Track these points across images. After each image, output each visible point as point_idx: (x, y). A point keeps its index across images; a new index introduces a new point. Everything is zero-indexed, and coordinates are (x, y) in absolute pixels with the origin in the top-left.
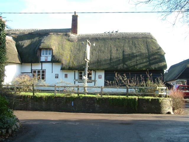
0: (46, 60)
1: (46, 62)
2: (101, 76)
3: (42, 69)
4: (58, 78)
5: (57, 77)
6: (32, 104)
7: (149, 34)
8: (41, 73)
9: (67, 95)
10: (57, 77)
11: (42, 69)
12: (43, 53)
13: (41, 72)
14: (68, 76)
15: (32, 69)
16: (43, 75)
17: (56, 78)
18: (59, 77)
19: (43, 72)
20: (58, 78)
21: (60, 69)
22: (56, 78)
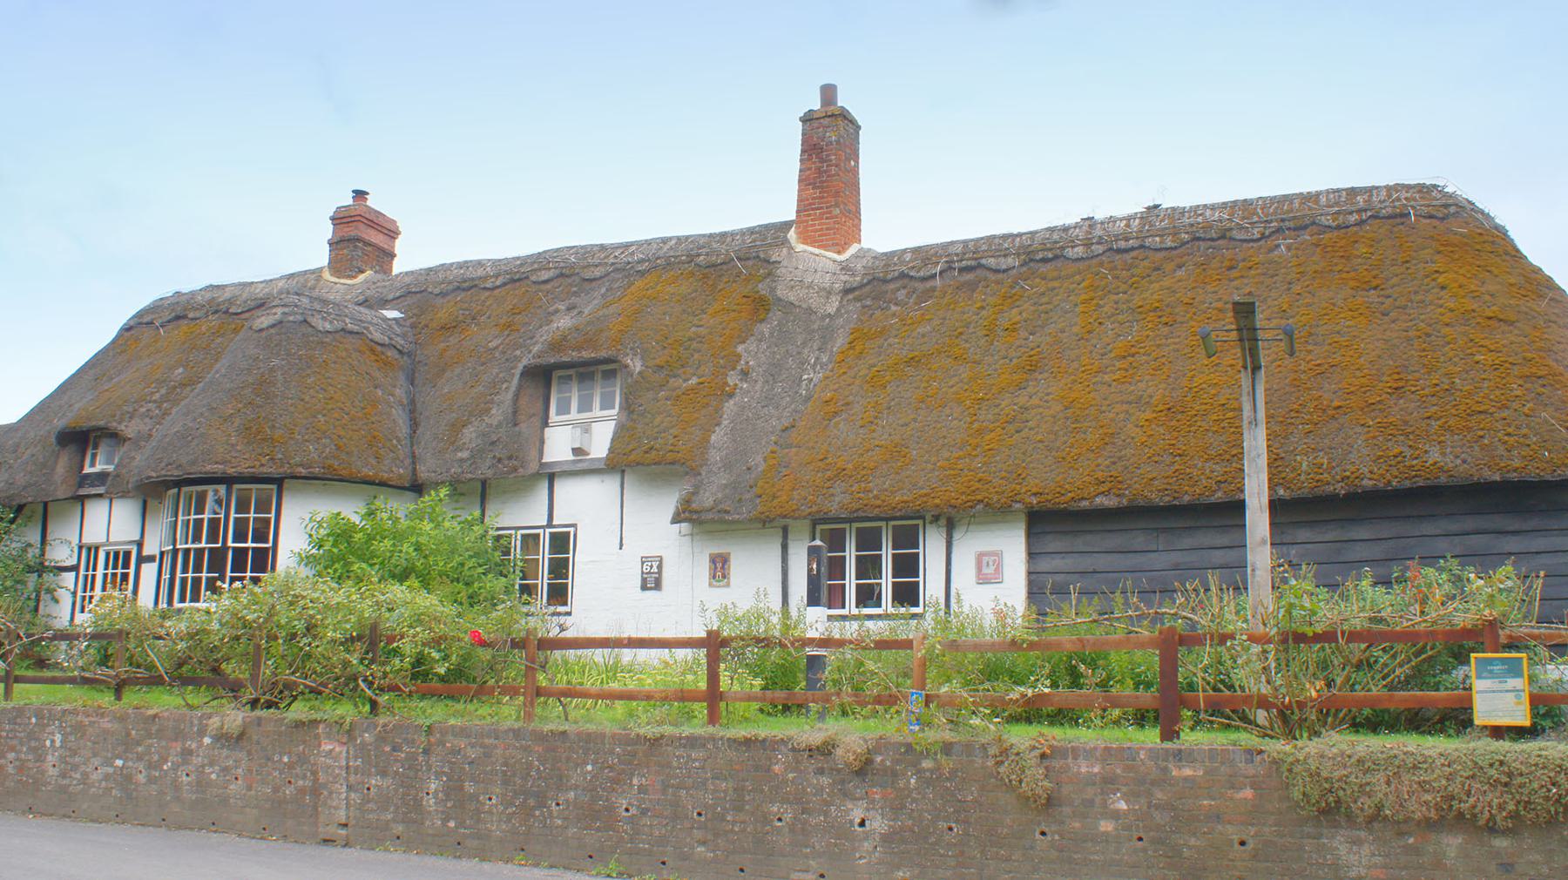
0: (577, 451)
1: (581, 468)
2: (998, 555)
3: (550, 524)
4: (658, 585)
5: (652, 581)
6: (350, 787)
7: (394, 222)
8: (545, 555)
9: (660, 723)
10: (652, 581)
11: (550, 524)
12: (559, 400)
13: (545, 543)
14: (736, 568)
15: (84, 541)
16: (560, 568)
17: (644, 587)
18: (665, 582)
19: (561, 542)
20: (658, 585)
21: (670, 518)
22: (644, 587)
